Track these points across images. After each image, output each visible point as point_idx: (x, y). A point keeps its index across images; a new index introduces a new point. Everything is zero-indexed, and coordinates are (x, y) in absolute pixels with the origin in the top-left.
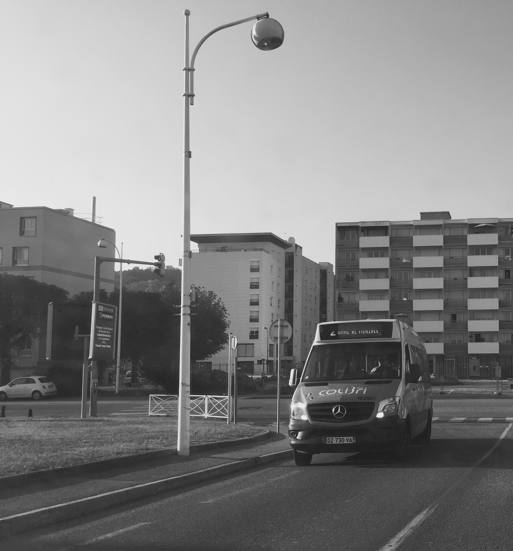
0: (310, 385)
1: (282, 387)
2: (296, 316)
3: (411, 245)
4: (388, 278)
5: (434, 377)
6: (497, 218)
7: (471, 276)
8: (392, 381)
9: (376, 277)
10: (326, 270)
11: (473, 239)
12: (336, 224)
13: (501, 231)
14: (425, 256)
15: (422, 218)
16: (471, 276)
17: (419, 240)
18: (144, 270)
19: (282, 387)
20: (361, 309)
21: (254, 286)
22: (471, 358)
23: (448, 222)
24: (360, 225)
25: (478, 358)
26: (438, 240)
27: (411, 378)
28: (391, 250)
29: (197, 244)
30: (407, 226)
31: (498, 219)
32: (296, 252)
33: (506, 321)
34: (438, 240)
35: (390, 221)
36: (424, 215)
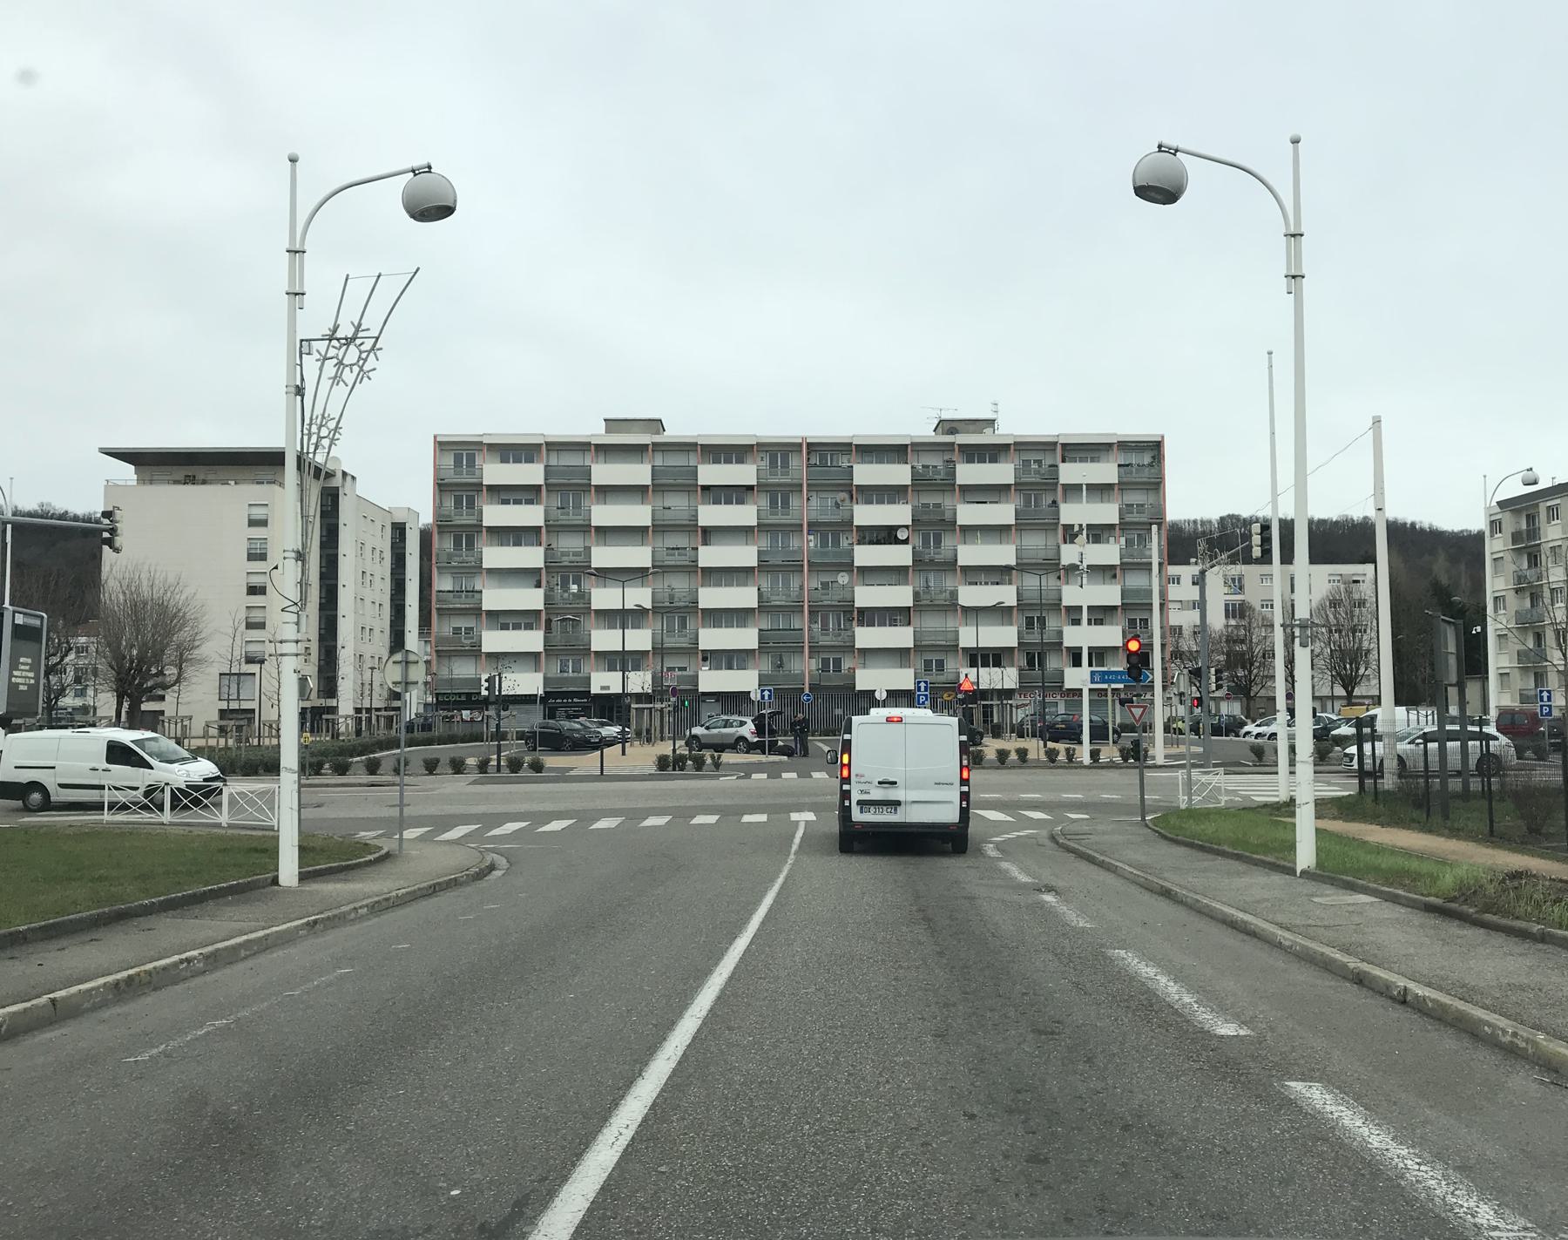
0: (1291, 739)
1: (820, 744)
2: (344, 616)
3: (850, 481)
4: (540, 545)
5: (1436, 729)
6: (1012, 435)
7: (705, 543)
8: (132, 741)
9: (517, 543)
10: (405, 523)
11: (710, 474)
12: (435, 437)
13: (762, 460)
14: (1072, 502)
15: (608, 431)
16: (707, 545)
17: (604, 473)
18: (1355, 519)
19: (820, 744)
20: (487, 605)
21: (257, 556)
22: (704, 701)
23: (658, 439)
24: (486, 440)
25: (717, 701)
26: (639, 473)
27: (1422, 730)
28: (548, 491)
29: (133, 467)
30: (582, 447)
31: (911, 437)
32: (343, 486)
33: (771, 630)
34: (639, 473)
35: (758, 435)
36: (612, 424)
